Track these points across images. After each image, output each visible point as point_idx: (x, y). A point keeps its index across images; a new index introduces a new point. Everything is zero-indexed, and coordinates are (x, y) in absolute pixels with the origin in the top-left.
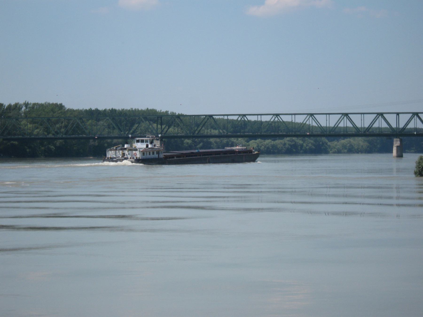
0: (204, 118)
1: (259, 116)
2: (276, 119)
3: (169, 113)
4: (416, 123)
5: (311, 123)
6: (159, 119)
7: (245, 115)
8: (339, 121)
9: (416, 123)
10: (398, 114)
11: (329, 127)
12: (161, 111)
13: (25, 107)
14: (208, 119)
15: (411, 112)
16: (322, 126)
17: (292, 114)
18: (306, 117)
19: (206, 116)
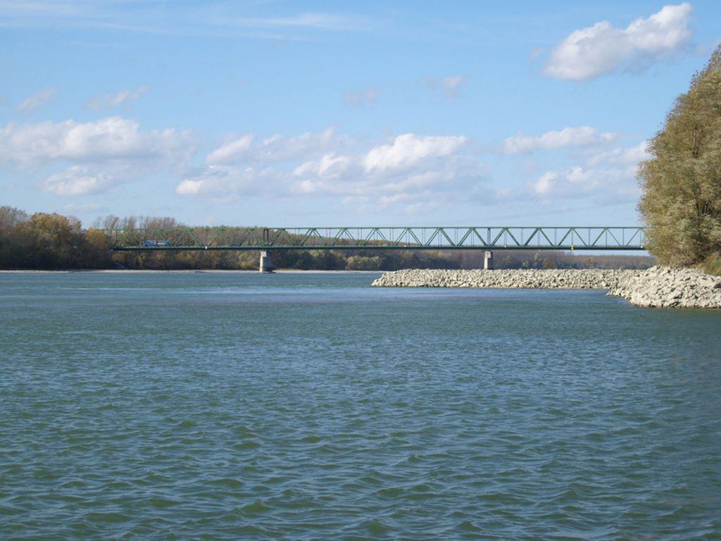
0: (277, 232)
1: (297, 230)
2: (313, 234)
3: (137, 226)
4: (506, 239)
5: (344, 237)
6: (266, 231)
7: (314, 229)
8: (401, 236)
9: (506, 239)
10: (489, 229)
11: (330, 238)
12: (71, 229)
13: (320, 255)
14: (249, 233)
15: (404, 226)
16: (321, 235)
17: (358, 228)
18: (416, 230)
19: (278, 229)
